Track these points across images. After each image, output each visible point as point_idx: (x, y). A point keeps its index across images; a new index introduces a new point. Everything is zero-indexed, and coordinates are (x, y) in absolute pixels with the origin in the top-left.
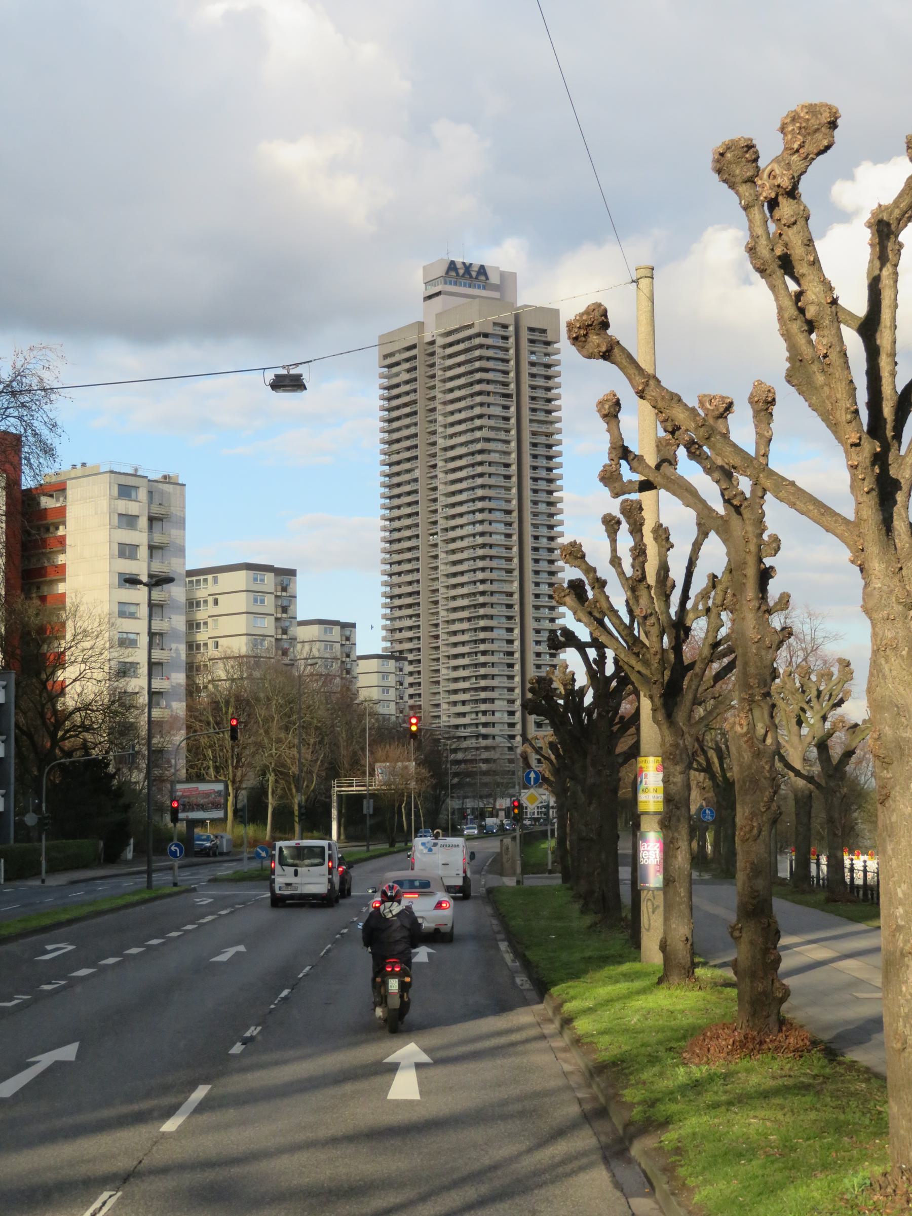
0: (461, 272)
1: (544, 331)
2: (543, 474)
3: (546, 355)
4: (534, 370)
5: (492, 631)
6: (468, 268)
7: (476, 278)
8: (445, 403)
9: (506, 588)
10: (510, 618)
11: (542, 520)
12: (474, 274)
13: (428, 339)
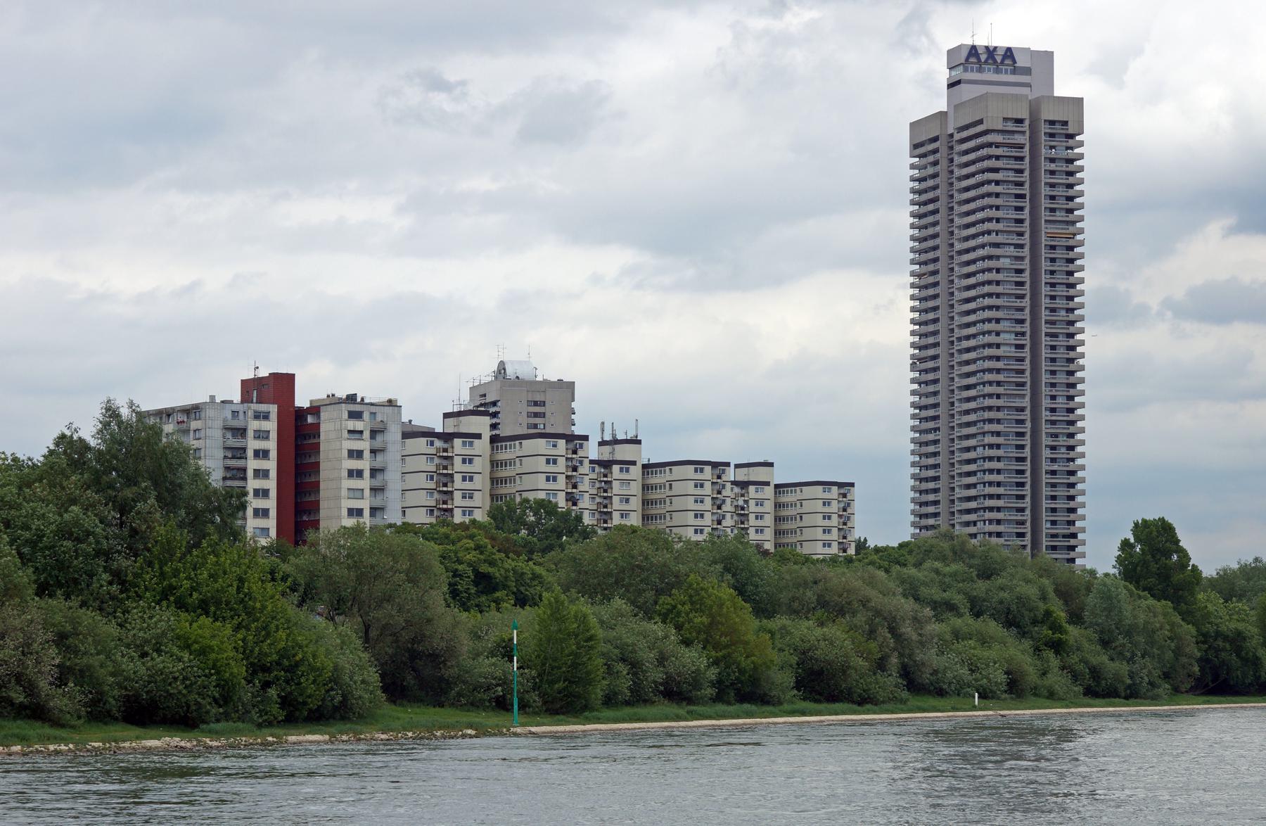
1: (1065, 123)
2: (1060, 278)
3: (1067, 148)
4: (1053, 167)
6: (991, 51)
7: (1002, 62)
9: (1018, 403)
12: (999, 59)
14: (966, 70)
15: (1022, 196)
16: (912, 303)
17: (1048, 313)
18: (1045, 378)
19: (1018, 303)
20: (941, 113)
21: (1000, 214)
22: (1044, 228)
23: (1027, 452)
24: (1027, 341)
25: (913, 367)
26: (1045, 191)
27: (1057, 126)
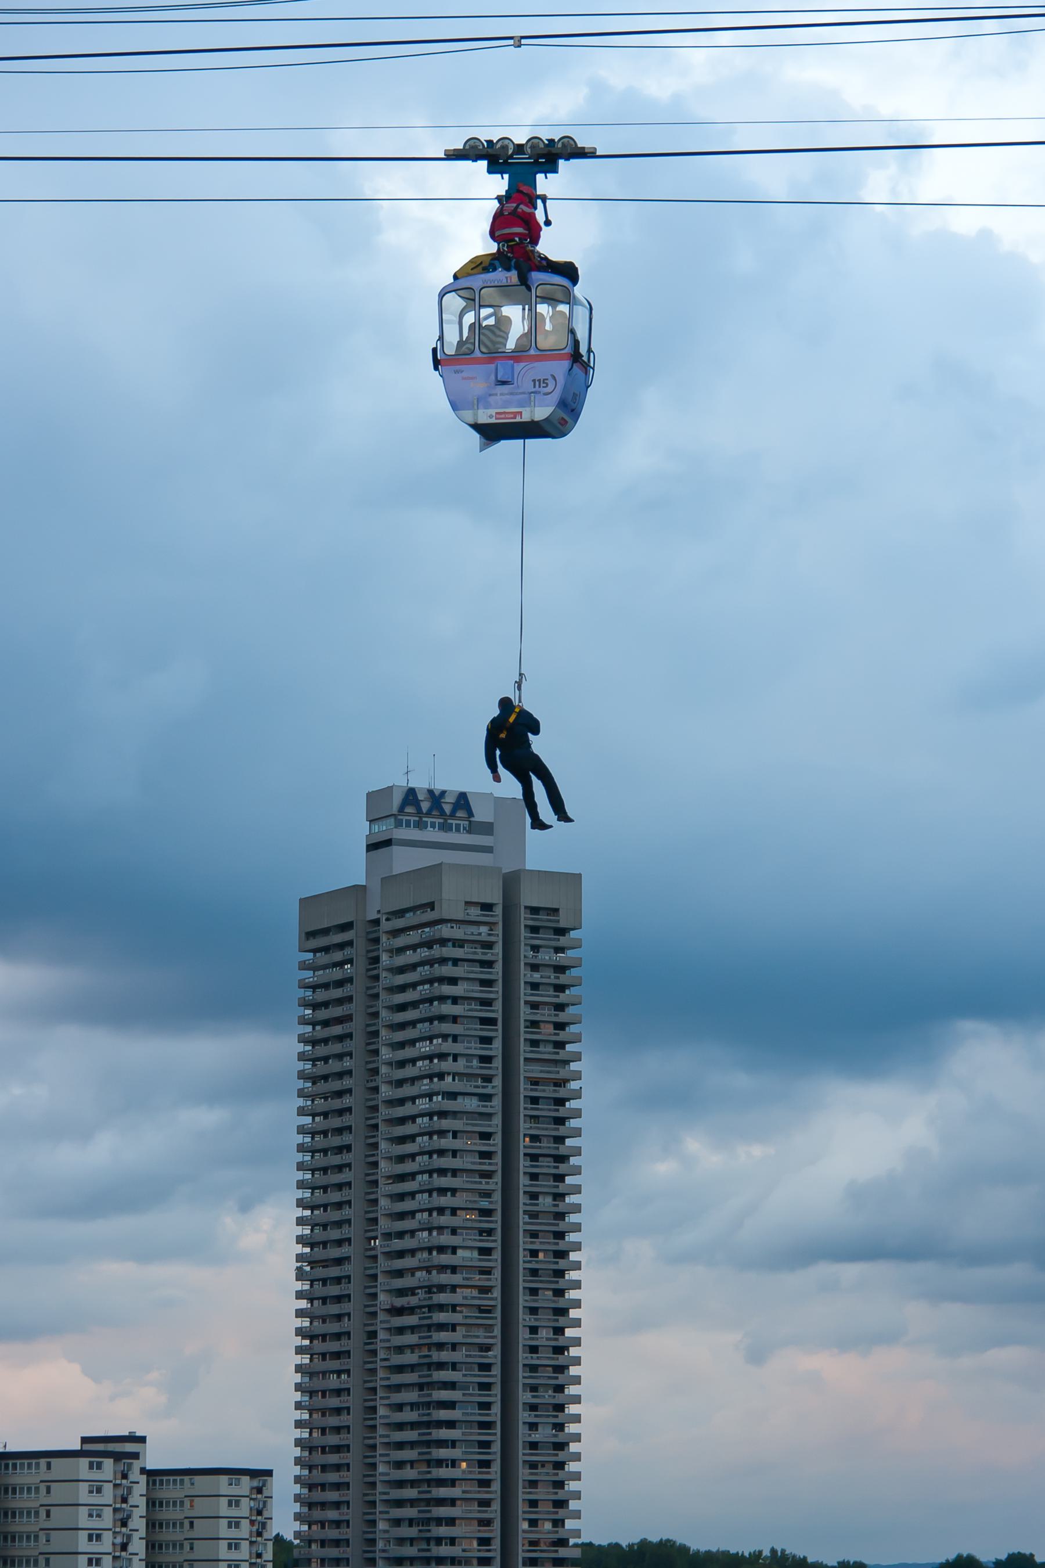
0: (425, 806)
1: (555, 911)
3: (559, 950)
4: (536, 977)
5: (453, 1486)
6: (436, 798)
7: (453, 815)
10: (485, 1387)
11: (547, 996)
12: (447, 809)
13: (373, 915)
14: (399, 824)
15: (492, 1022)
16: (300, 1175)
18: (523, 1300)
20: (356, 887)
22: (524, 1071)
23: (496, 1413)
25: (300, 1275)
26: (524, 1013)
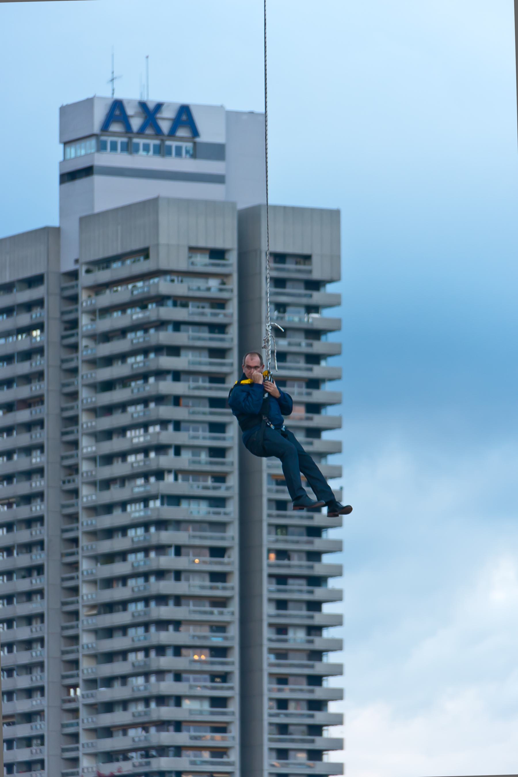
0: (136, 123)
1: (307, 258)
2: (297, 565)
3: (311, 309)
4: (283, 344)
6: (150, 113)
7: (172, 134)
8: (95, 363)
12: (165, 126)
13: (68, 266)
14: (102, 147)
17: (272, 658)
19: (217, 615)
21: (181, 438)
24: (232, 690)
27: (290, 265)
